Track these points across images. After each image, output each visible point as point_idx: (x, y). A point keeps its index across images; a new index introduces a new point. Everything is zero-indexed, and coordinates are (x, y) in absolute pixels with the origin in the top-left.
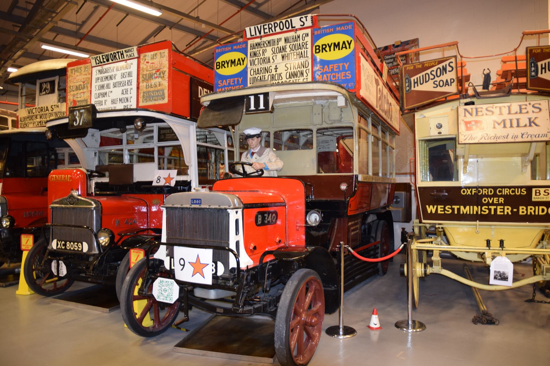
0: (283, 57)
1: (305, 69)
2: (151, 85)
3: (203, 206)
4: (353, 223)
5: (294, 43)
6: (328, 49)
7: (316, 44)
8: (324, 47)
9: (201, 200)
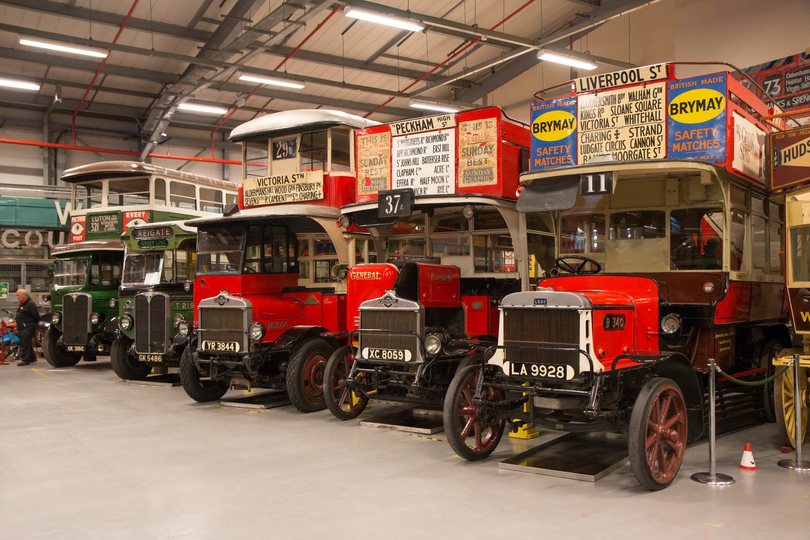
0: (626, 119)
1: (656, 136)
2: (474, 162)
3: (549, 307)
4: (722, 335)
5: (642, 101)
6: (688, 109)
7: (673, 102)
8: (683, 106)
9: (546, 300)
